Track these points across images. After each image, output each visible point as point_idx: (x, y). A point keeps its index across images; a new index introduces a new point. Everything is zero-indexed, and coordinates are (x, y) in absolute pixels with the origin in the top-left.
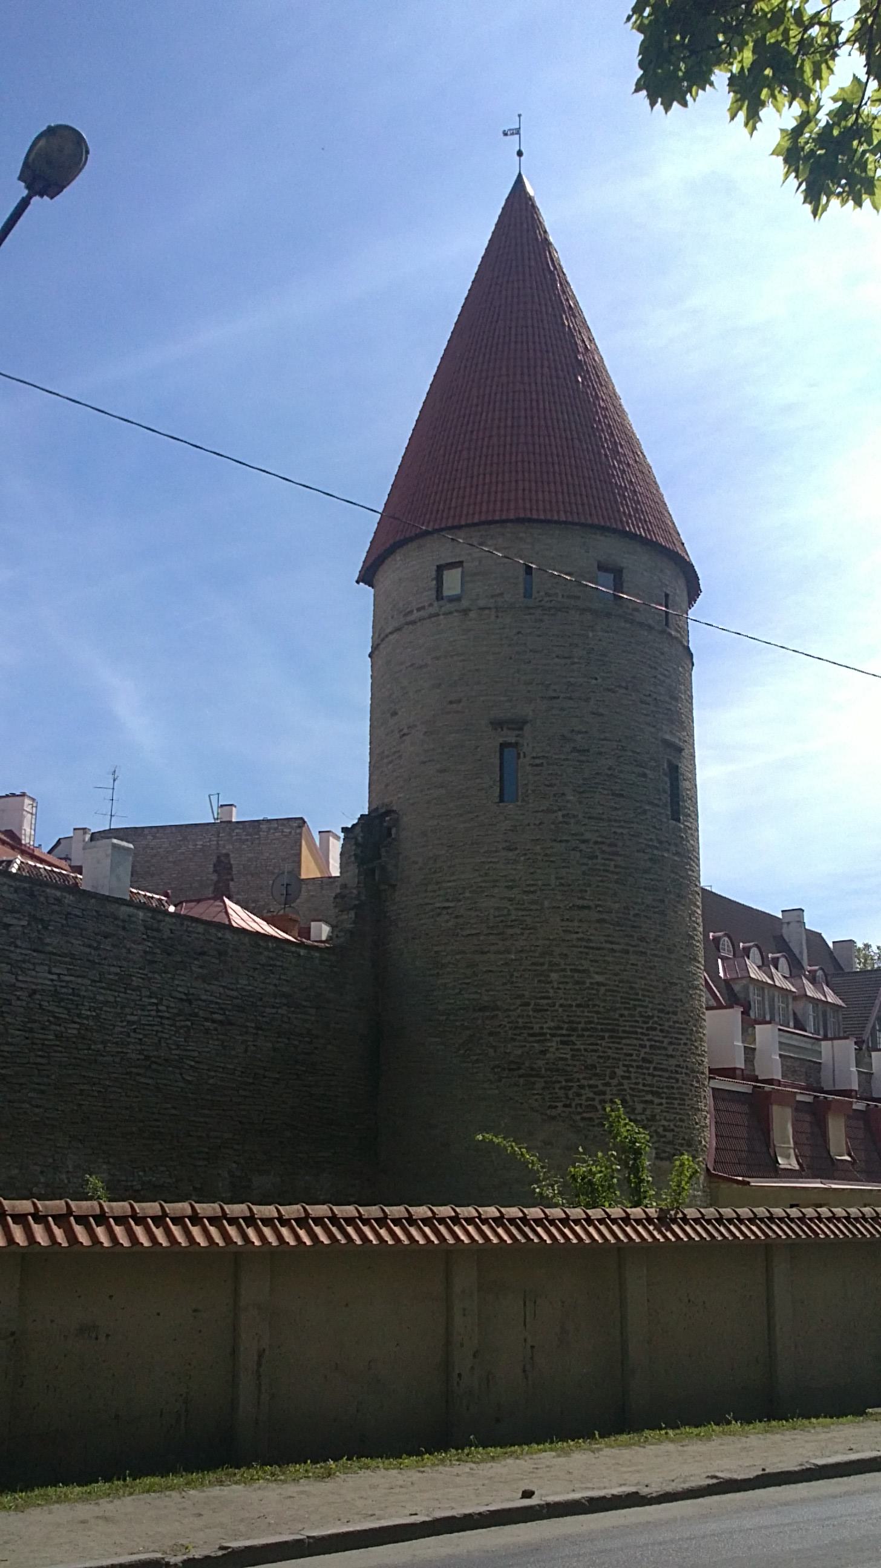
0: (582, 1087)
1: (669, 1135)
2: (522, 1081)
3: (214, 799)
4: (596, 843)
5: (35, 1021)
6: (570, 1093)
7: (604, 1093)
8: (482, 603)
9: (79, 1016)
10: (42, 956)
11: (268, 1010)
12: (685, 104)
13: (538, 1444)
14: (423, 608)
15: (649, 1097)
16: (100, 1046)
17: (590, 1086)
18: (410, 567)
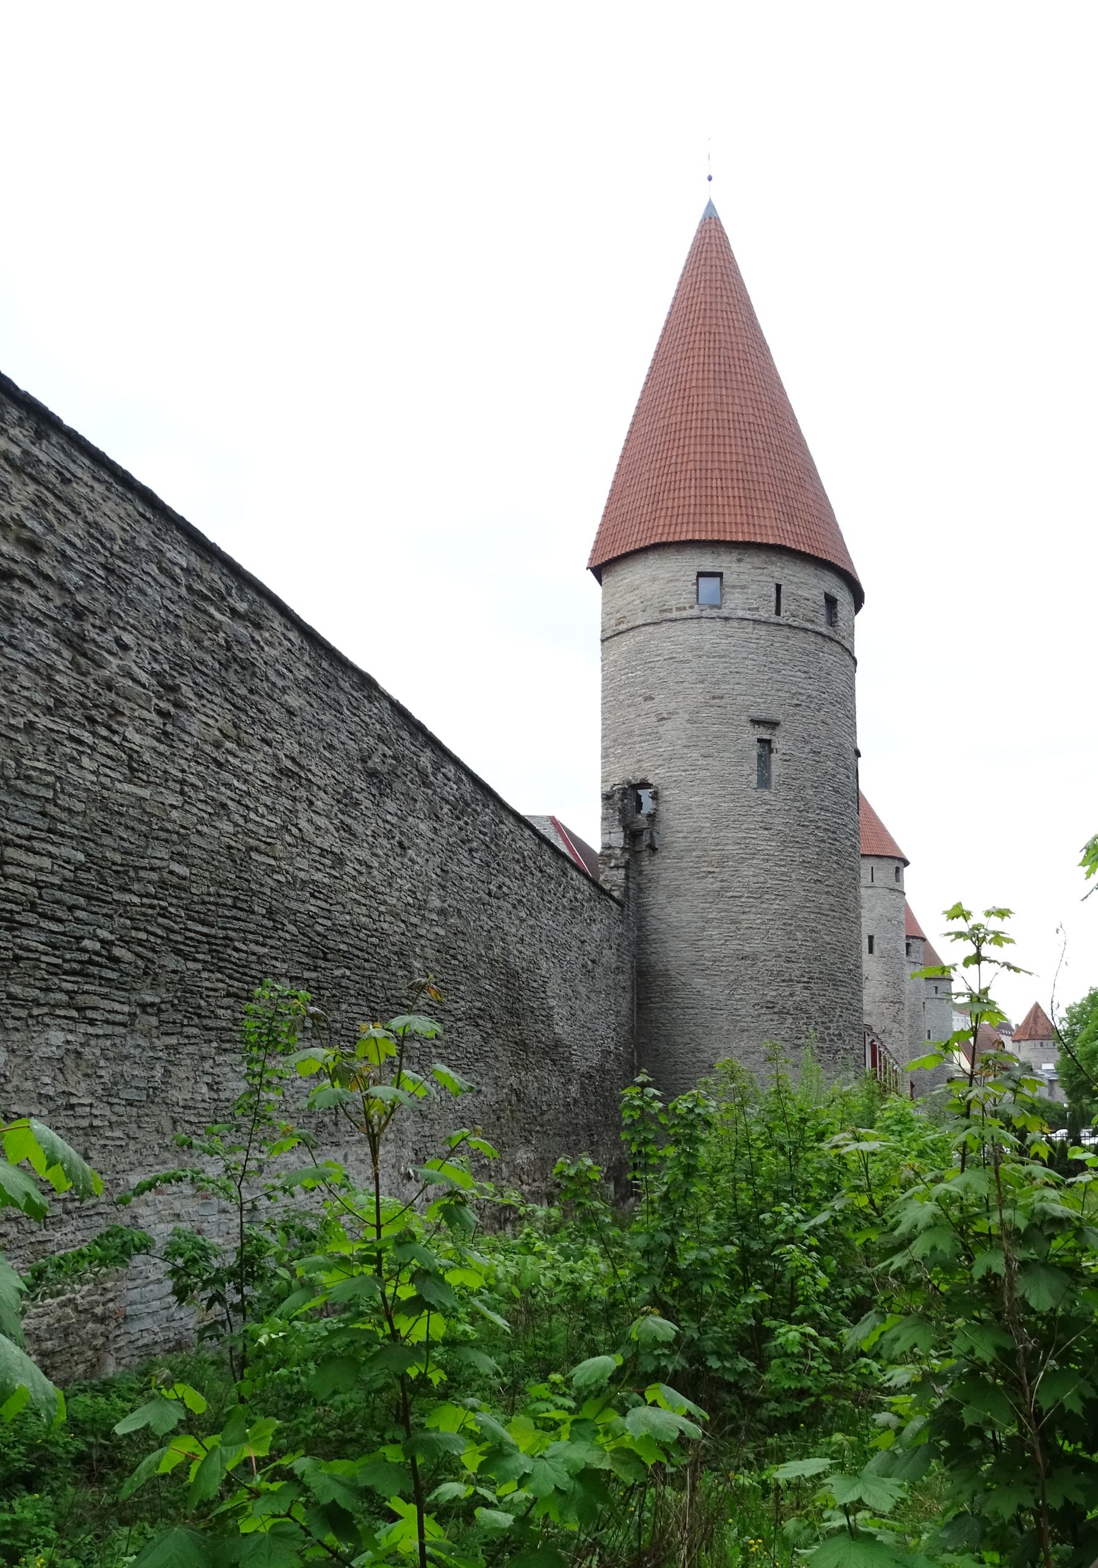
0: (817, 1023)
2: (776, 1017)
8: (740, 613)
13: (775, 1416)
14: (685, 609)
17: (823, 1023)
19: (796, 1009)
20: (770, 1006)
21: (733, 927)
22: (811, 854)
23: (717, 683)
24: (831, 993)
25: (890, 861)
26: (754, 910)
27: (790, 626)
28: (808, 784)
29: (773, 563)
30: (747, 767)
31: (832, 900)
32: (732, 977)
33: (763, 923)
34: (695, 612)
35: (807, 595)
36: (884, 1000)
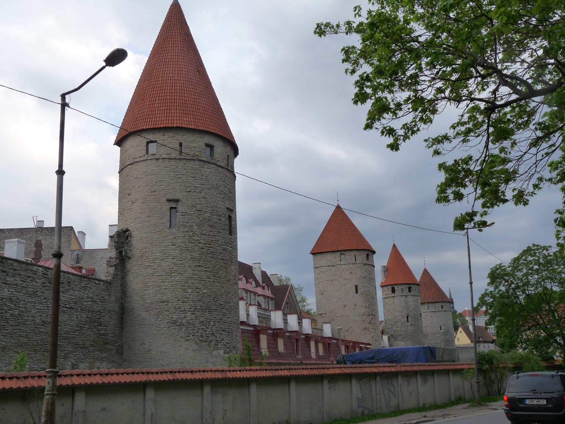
0: (199, 329)
1: (228, 345)
2: (177, 327)
3: (35, 218)
4: (204, 243)
5: (3, 309)
6: (195, 332)
7: (206, 331)
8: (164, 156)
9: (19, 307)
10: (6, 285)
11: (85, 303)
12: (462, 214)
14: (141, 157)
15: (221, 332)
16: (26, 318)
17: (202, 329)
18: (136, 144)
19: (187, 323)
20: (175, 322)
21: (158, 289)
22: (196, 255)
23: (153, 186)
24: (207, 315)
25: (364, 251)
26: (168, 281)
27: (186, 159)
28: (194, 224)
29: (178, 134)
30: (165, 219)
31: (208, 274)
32: (158, 310)
33: (172, 286)
34: (145, 158)
35: (195, 146)
36: (364, 314)
